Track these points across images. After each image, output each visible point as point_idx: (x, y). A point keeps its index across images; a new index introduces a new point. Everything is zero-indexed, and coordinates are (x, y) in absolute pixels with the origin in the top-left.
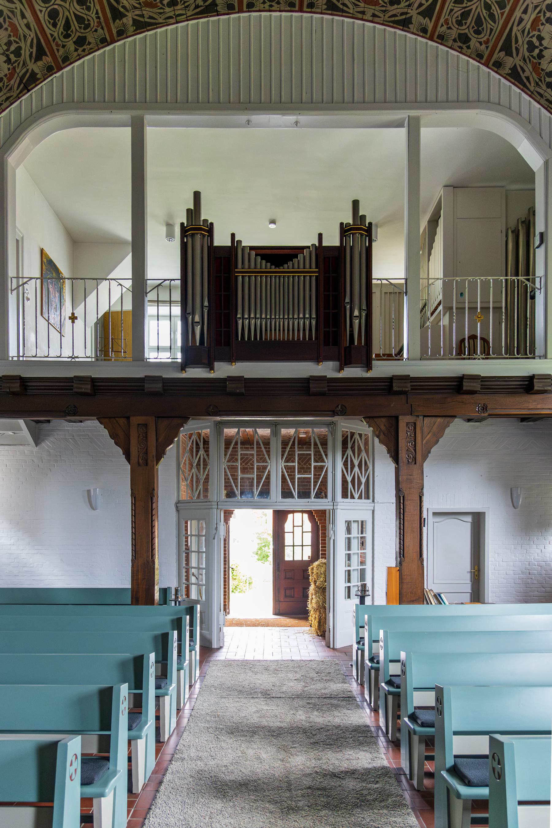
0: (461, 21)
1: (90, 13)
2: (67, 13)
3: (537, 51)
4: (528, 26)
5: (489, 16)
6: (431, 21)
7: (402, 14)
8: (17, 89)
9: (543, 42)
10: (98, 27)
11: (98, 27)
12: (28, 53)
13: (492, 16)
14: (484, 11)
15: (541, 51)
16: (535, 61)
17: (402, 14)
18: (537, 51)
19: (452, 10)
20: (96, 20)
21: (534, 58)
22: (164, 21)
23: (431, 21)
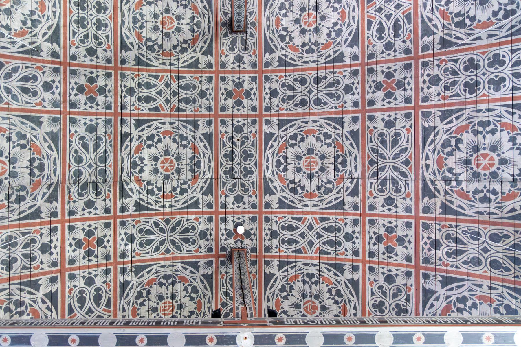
0: (382, 188)
1: (292, 106)
2: (300, 90)
3: (334, 293)
4: (348, 307)
5: (396, 154)
6: (423, 287)
7: (275, 45)
8: (353, 296)
9: (333, 301)
10: (407, 38)
11: (407, 38)
12: (345, 38)
13: (403, 174)
14: (177, 230)
15: (331, 295)
16: (331, 286)
17: (275, 45)
18: (334, 293)
19: (187, 251)
20: (107, 192)
21: (333, 287)
22: (11, 117)
23: (423, 287)
